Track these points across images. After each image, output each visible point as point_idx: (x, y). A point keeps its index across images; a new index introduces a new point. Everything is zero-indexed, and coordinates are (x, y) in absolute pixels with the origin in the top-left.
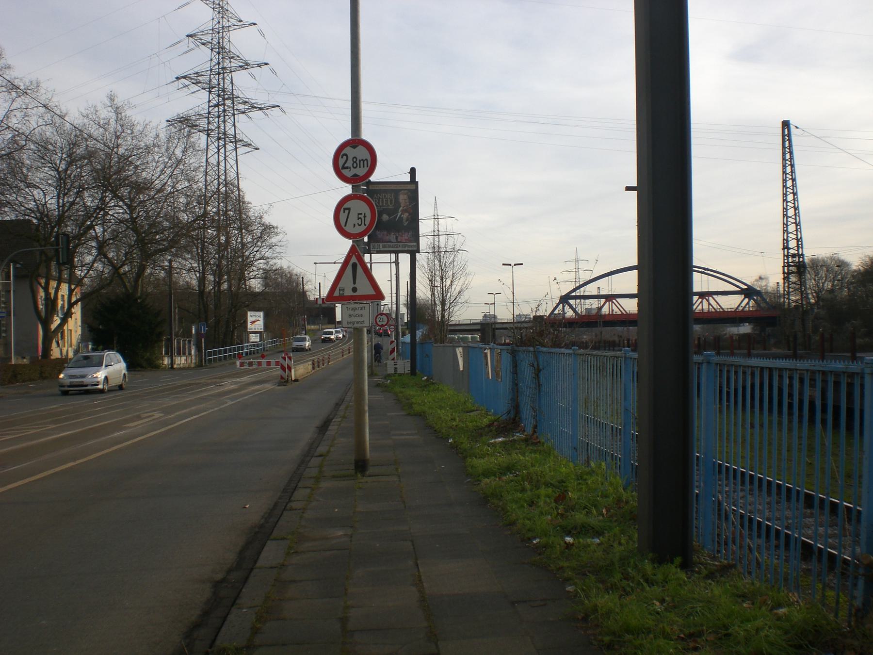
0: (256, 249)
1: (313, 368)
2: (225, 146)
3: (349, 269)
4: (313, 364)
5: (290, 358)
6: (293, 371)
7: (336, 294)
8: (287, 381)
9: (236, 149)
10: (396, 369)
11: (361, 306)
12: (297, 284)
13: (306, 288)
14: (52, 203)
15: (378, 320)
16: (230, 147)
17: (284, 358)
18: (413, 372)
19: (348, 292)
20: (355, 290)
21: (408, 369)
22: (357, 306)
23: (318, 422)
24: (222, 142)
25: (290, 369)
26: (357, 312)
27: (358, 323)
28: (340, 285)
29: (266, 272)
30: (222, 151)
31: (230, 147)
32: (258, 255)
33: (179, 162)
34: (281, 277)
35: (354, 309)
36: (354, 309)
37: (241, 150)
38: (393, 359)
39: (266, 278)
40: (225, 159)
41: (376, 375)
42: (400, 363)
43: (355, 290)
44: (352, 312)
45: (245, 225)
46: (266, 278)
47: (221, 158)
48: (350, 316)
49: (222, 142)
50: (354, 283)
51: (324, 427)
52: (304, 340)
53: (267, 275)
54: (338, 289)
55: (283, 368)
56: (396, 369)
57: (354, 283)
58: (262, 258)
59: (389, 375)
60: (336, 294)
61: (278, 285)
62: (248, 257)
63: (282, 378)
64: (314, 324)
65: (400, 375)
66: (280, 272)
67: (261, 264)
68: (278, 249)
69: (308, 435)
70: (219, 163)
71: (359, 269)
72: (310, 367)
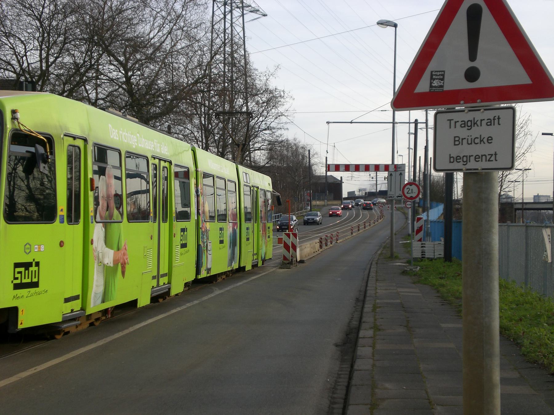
0: (261, 119)
1: (321, 247)
2: (231, 11)
3: (460, 21)
4: (321, 242)
5: (295, 235)
6: (298, 250)
7: (423, 86)
8: (291, 263)
9: (243, 15)
10: (423, 252)
11: (490, 115)
12: (303, 157)
13: (312, 161)
14: (33, 58)
15: (406, 191)
16: (237, 13)
17: (288, 235)
18: (448, 256)
19: (455, 81)
20: (472, 74)
21: (440, 252)
22: (478, 116)
23: (336, 334)
24: (228, 8)
25: (294, 247)
26: (476, 132)
27: (478, 158)
28: (433, 66)
29: (271, 143)
30: (228, 17)
31: (237, 13)
32: (263, 126)
33: (179, 17)
34: (287, 150)
35: (469, 125)
36: (469, 125)
37: (249, 16)
38: (420, 240)
39: (270, 150)
40: (232, 25)
41: (396, 258)
42: (429, 244)
43: (472, 74)
44: (463, 133)
45: (250, 91)
46: (270, 150)
47: (228, 25)
48: (457, 141)
49: (228, 8)
50: (473, 56)
51: (349, 344)
52: (317, 215)
53: (274, 147)
54: (426, 76)
55: (286, 247)
56: (423, 252)
57: (473, 56)
58: (268, 128)
59: (415, 259)
60: (423, 86)
61: (283, 158)
62: (253, 127)
63: (285, 258)
64: (319, 199)
65: (431, 260)
66: (285, 144)
67: (266, 135)
68: (283, 119)
69: (325, 365)
70: (225, 30)
71: (488, 21)
72: (318, 245)
